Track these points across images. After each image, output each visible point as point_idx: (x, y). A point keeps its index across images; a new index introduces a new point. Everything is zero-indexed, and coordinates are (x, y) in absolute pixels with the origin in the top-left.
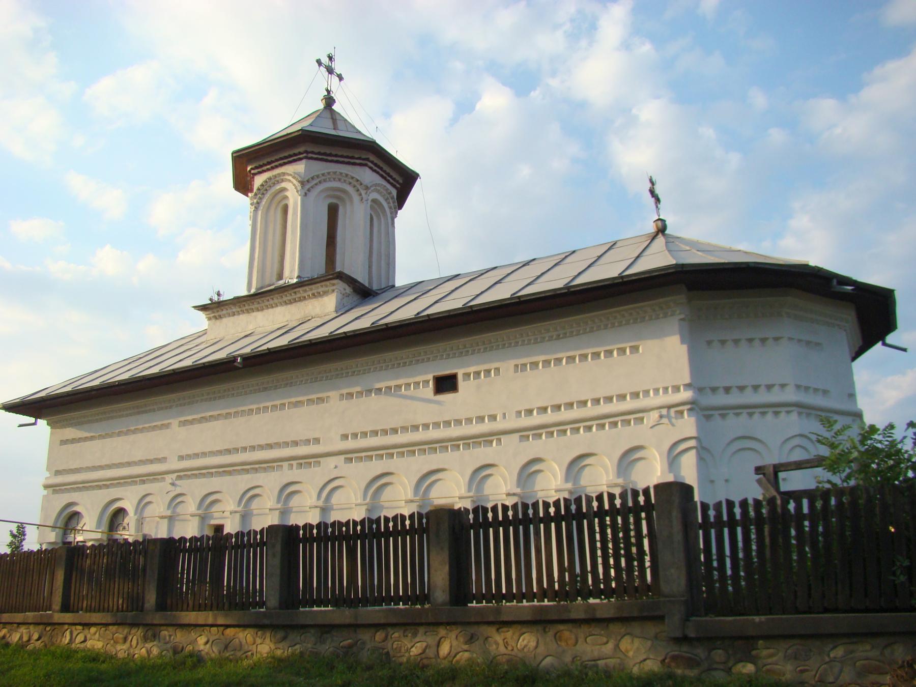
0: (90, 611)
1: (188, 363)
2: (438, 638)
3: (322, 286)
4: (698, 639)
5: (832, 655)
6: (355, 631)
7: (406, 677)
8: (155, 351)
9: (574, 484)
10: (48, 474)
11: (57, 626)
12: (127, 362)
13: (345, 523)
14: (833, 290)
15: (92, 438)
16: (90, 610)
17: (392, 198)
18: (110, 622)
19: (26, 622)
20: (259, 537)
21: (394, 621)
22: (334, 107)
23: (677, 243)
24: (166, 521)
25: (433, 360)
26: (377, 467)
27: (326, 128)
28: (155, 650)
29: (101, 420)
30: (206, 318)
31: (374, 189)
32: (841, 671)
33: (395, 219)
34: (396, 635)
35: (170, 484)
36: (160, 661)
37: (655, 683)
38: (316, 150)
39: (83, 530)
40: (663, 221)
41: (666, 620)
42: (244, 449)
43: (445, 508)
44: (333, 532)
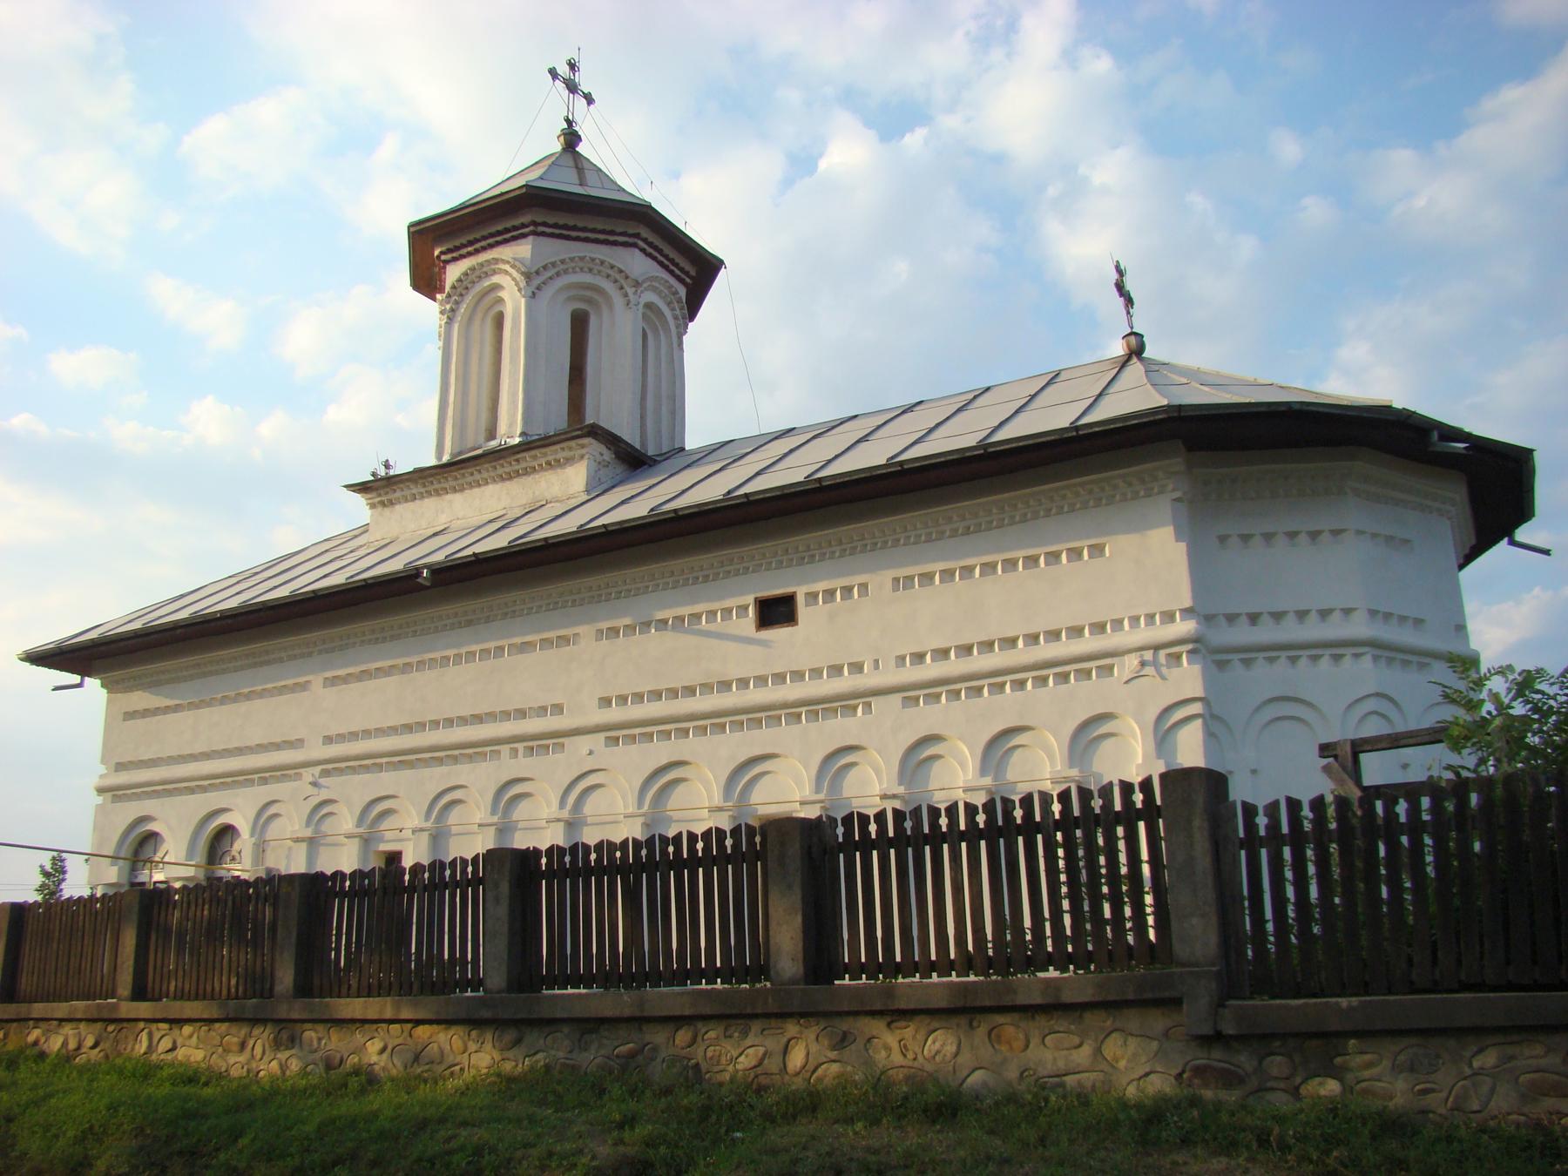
0: (182, 998)
1: (338, 579)
2: (785, 1040)
3: (563, 449)
4: (1242, 1039)
5: (1476, 1064)
6: (641, 1029)
7: (731, 1107)
8: (160, 608)
9: (995, 779)
10: (102, 769)
11: (125, 1025)
12: (234, 580)
13: (620, 843)
14: (1431, 449)
15: (177, 708)
16: (181, 996)
17: (680, 300)
18: (216, 1016)
19: (72, 1017)
20: (470, 869)
21: (707, 1011)
22: (580, 149)
23: (1165, 372)
24: (304, 846)
25: (753, 572)
26: (661, 752)
27: (566, 182)
28: (294, 1064)
29: (192, 678)
30: (367, 504)
31: (649, 286)
32: (1493, 1090)
33: (684, 337)
34: (712, 1034)
35: (310, 783)
36: (304, 1082)
37: (1168, 1114)
38: (551, 221)
39: (164, 863)
40: (1139, 336)
41: (1185, 1006)
42: (435, 724)
43: (781, 817)
44: (599, 860)
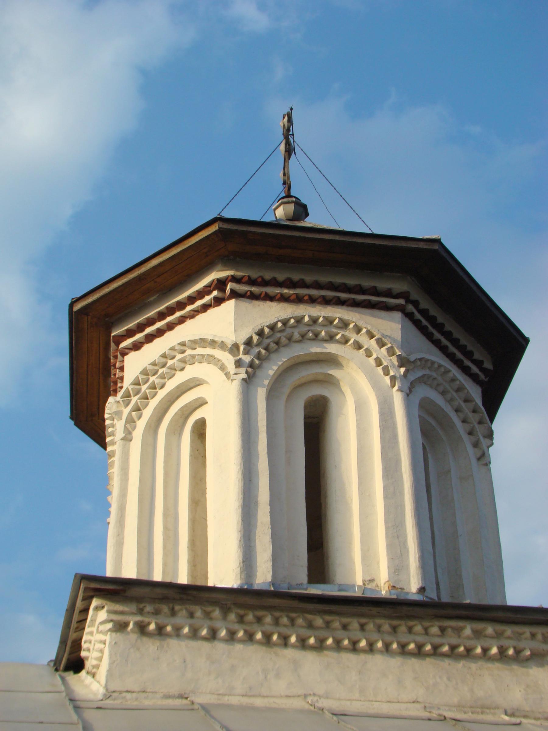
3: (533, 636)
